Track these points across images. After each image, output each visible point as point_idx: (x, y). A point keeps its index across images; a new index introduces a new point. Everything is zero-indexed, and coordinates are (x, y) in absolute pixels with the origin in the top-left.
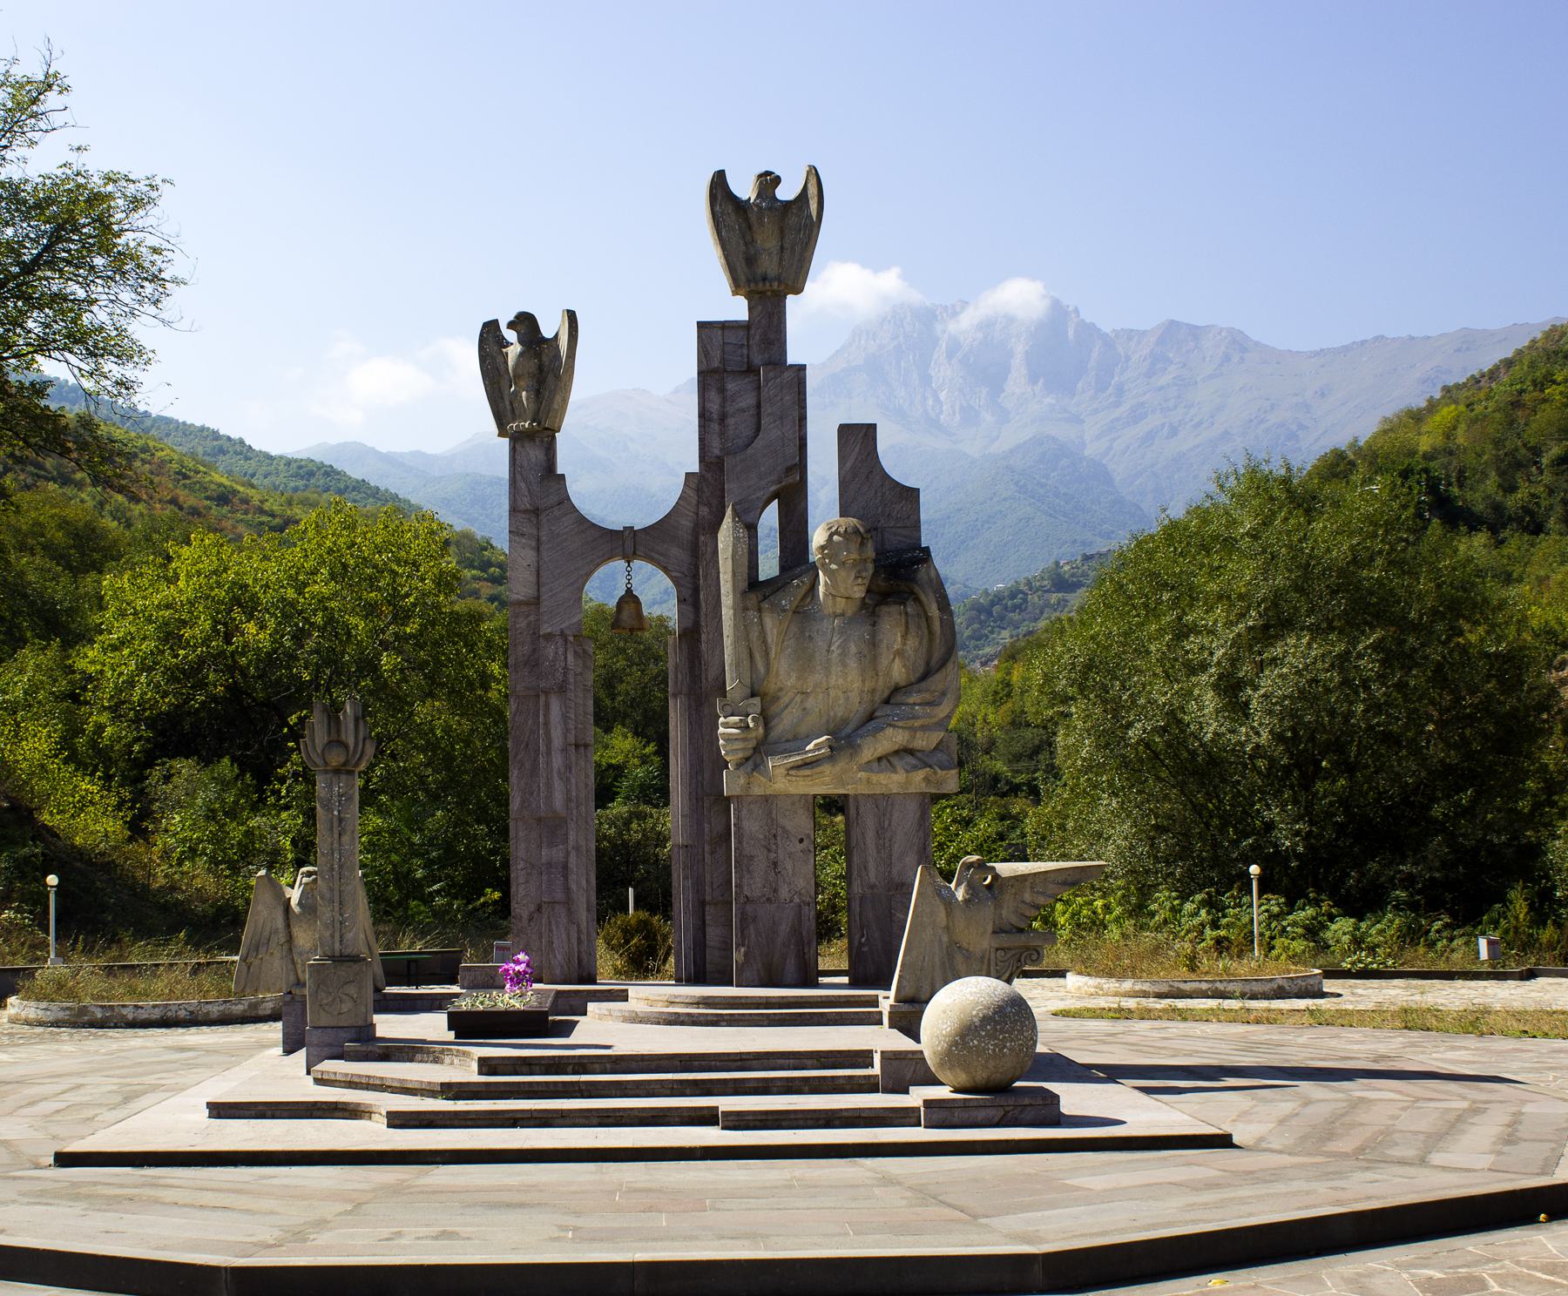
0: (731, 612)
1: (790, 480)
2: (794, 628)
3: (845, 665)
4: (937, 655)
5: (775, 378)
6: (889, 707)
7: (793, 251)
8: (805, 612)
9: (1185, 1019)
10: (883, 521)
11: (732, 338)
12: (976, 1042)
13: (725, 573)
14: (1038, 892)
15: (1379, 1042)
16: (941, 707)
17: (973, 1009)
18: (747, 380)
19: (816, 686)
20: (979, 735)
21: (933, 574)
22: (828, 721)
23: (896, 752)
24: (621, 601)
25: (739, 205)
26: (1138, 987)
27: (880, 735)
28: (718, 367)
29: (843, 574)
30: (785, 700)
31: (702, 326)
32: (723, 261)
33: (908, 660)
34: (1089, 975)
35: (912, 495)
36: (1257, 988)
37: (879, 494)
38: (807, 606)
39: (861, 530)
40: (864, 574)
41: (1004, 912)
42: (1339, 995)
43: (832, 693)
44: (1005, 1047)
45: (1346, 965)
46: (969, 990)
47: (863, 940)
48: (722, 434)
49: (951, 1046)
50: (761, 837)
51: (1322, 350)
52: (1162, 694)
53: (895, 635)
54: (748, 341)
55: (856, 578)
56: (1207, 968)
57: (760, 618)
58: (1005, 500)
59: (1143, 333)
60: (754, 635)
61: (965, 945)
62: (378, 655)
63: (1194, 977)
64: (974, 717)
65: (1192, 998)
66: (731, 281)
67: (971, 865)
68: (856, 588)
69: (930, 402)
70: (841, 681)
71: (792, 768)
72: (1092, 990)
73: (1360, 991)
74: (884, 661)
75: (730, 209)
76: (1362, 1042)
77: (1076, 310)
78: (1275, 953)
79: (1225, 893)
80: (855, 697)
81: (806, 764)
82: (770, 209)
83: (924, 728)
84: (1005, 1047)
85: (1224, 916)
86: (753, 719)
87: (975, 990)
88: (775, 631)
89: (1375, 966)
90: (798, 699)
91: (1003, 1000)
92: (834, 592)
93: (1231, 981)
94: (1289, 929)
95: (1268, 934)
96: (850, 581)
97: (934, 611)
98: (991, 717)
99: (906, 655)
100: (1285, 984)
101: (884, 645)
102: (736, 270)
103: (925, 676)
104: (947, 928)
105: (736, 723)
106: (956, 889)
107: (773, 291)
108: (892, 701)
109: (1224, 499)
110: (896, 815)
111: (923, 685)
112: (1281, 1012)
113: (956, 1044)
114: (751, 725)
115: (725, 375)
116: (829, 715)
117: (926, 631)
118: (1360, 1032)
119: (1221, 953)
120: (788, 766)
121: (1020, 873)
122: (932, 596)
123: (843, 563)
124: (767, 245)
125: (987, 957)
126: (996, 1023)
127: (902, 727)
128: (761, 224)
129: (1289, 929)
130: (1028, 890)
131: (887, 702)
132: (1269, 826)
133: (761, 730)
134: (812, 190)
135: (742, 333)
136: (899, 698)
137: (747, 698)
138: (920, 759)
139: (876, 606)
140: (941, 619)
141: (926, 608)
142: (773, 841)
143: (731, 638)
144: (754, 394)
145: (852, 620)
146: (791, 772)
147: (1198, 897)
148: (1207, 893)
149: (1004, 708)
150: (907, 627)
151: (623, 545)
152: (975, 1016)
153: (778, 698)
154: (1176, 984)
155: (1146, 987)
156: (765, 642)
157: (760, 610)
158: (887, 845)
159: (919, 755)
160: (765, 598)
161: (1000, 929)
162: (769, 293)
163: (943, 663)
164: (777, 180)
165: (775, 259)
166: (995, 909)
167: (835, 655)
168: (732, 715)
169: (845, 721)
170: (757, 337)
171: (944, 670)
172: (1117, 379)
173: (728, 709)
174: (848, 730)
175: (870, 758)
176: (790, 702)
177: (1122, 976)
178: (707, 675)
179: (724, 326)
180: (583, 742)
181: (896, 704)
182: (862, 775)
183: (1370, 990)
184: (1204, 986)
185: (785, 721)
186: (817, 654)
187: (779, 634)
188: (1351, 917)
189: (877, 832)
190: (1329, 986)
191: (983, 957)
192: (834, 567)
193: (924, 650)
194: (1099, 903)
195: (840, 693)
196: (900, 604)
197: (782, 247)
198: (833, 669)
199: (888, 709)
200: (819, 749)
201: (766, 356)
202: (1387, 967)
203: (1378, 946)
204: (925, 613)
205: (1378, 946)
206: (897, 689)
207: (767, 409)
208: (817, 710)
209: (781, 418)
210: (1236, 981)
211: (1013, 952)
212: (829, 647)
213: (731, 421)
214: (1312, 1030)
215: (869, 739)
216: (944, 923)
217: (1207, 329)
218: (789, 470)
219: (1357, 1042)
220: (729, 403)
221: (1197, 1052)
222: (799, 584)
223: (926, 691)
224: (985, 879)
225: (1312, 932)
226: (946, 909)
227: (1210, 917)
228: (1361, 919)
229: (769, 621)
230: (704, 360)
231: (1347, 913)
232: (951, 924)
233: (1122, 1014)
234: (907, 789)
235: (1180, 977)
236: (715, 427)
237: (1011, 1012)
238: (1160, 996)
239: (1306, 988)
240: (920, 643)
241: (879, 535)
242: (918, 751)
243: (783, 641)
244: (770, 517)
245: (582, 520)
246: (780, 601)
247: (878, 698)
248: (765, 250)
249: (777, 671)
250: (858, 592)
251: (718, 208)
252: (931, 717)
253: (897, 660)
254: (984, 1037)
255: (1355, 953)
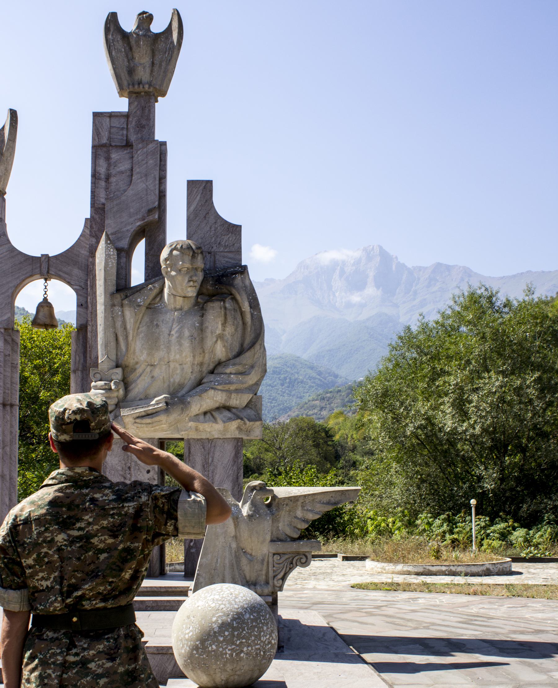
0: (103, 307)
1: (151, 218)
2: (146, 319)
3: (180, 345)
4: (248, 340)
5: (143, 148)
6: (213, 375)
7: (160, 65)
8: (155, 308)
9: (430, 591)
10: (215, 248)
11: (116, 123)
12: (214, 647)
13: (100, 280)
14: (307, 510)
15: (554, 611)
16: (250, 377)
17: (213, 616)
18: (125, 152)
19: (160, 360)
20: (349, 443)
21: (247, 283)
22: (169, 386)
23: (218, 409)
24: (40, 307)
25: (125, 36)
26: (406, 568)
27: (205, 395)
28: (106, 143)
29: (179, 278)
30: (139, 370)
31: (97, 115)
32: (112, 71)
33: (227, 342)
34: (378, 561)
35: (236, 230)
36: (474, 569)
37: (213, 229)
38: (157, 304)
39: (194, 247)
40: (194, 278)
41: (280, 525)
42: (520, 573)
43: (172, 365)
44: (242, 651)
45: (523, 555)
46: (212, 597)
47: (192, 544)
48: (107, 189)
49: (193, 650)
50: (119, 468)
51: (504, 277)
52: (423, 407)
53: (217, 323)
54: (127, 126)
55: (189, 281)
56: (446, 557)
57: (123, 312)
58: (364, 341)
59: (425, 268)
60: (119, 324)
61: (249, 551)
62: (39, 392)
63: (438, 562)
64: (347, 435)
65: (436, 575)
66: (117, 85)
67: (254, 488)
68: (189, 289)
69: (332, 297)
70: (178, 356)
71: (138, 417)
72: (380, 570)
73: (532, 571)
74: (209, 343)
75: (119, 37)
76: (543, 611)
77: (396, 258)
78: (483, 548)
79: (457, 515)
80: (188, 369)
81: (148, 415)
82: (145, 36)
83: (237, 391)
84: (242, 651)
85: (456, 527)
86: (115, 383)
87: (217, 597)
88: (132, 320)
89: (539, 555)
90: (149, 369)
91: (243, 608)
92: (174, 293)
93: (459, 565)
94: (491, 534)
95: (479, 537)
96: (184, 284)
97: (246, 307)
98: (354, 436)
99: (226, 338)
100: (491, 568)
101: (209, 331)
102: (121, 79)
103: (239, 354)
104: (236, 537)
105: (102, 386)
106: (242, 507)
107: (145, 92)
108: (215, 372)
109: (458, 308)
110: (217, 454)
111: (237, 360)
112: (489, 585)
113: (196, 648)
114: (113, 387)
115: (110, 148)
116: (169, 381)
117: (241, 322)
118: (540, 602)
119: (454, 548)
120: (135, 416)
121: (293, 495)
122: (245, 297)
123: (180, 270)
124: (142, 61)
125: (266, 560)
126: (234, 629)
127: (221, 390)
128: (138, 45)
129: (491, 534)
130: (300, 508)
131: (212, 372)
132: (480, 478)
133: (121, 392)
134: (175, 25)
135: (123, 120)
136: (220, 369)
137: (112, 368)
138: (234, 414)
139: (205, 303)
140: (252, 315)
141: (241, 305)
142: (128, 472)
143: (103, 325)
144: (130, 161)
145: (188, 313)
146: (138, 421)
147: (442, 517)
148: (448, 515)
149: (360, 432)
150: (226, 318)
151: (40, 267)
152: (215, 622)
153: (135, 370)
154: (427, 567)
155: (410, 569)
156: (125, 328)
157: (122, 306)
158: (210, 475)
159: (234, 410)
160: (127, 297)
161: (278, 538)
162: (143, 94)
163: (253, 345)
164: (150, 18)
165: (148, 70)
166: (273, 522)
167: (174, 337)
168: (101, 380)
169: (181, 386)
170: (134, 123)
171: (252, 350)
172: (414, 288)
173: (98, 376)
174: (183, 392)
175: (198, 412)
176: (143, 372)
177: (397, 562)
178: (90, 355)
179: (111, 115)
180: (9, 402)
181: (218, 374)
182: (191, 424)
183: (538, 570)
184: (444, 568)
185: (139, 386)
186: (162, 337)
187: (135, 322)
188: (525, 528)
189: (204, 466)
190: (515, 567)
191: (263, 560)
192: (173, 273)
193: (239, 335)
194: (390, 520)
195: (177, 366)
196: (221, 301)
197: (153, 64)
198: (172, 348)
199: (212, 377)
200: (157, 404)
201: (139, 135)
202: (545, 556)
203: (539, 544)
204: (240, 308)
205: (539, 544)
206: (219, 364)
207: (136, 170)
208: (161, 378)
209: (146, 175)
210: (462, 565)
211: (287, 556)
212: (170, 332)
213: (113, 180)
214: (509, 601)
215: (197, 398)
216: (233, 534)
217: (454, 267)
218: (150, 211)
219: (540, 611)
220: (112, 167)
221: (434, 624)
222: (154, 288)
223: (239, 365)
224: (267, 499)
225: (504, 536)
226: (234, 522)
227: (449, 528)
228: (530, 529)
229: (128, 313)
230: (96, 138)
231: (522, 526)
232: (238, 534)
233: (394, 587)
234: (225, 434)
235: (430, 563)
236: (103, 184)
237: (249, 618)
238: (418, 574)
239: (503, 570)
240: (236, 330)
241: (212, 257)
242: (234, 408)
243: (138, 328)
244: (140, 249)
245: (13, 249)
246: (136, 299)
247: (205, 369)
248: (141, 64)
249: (134, 350)
250: (192, 292)
251: (110, 37)
252: (243, 383)
253: (219, 342)
254: (222, 642)
255: (528, 548)
